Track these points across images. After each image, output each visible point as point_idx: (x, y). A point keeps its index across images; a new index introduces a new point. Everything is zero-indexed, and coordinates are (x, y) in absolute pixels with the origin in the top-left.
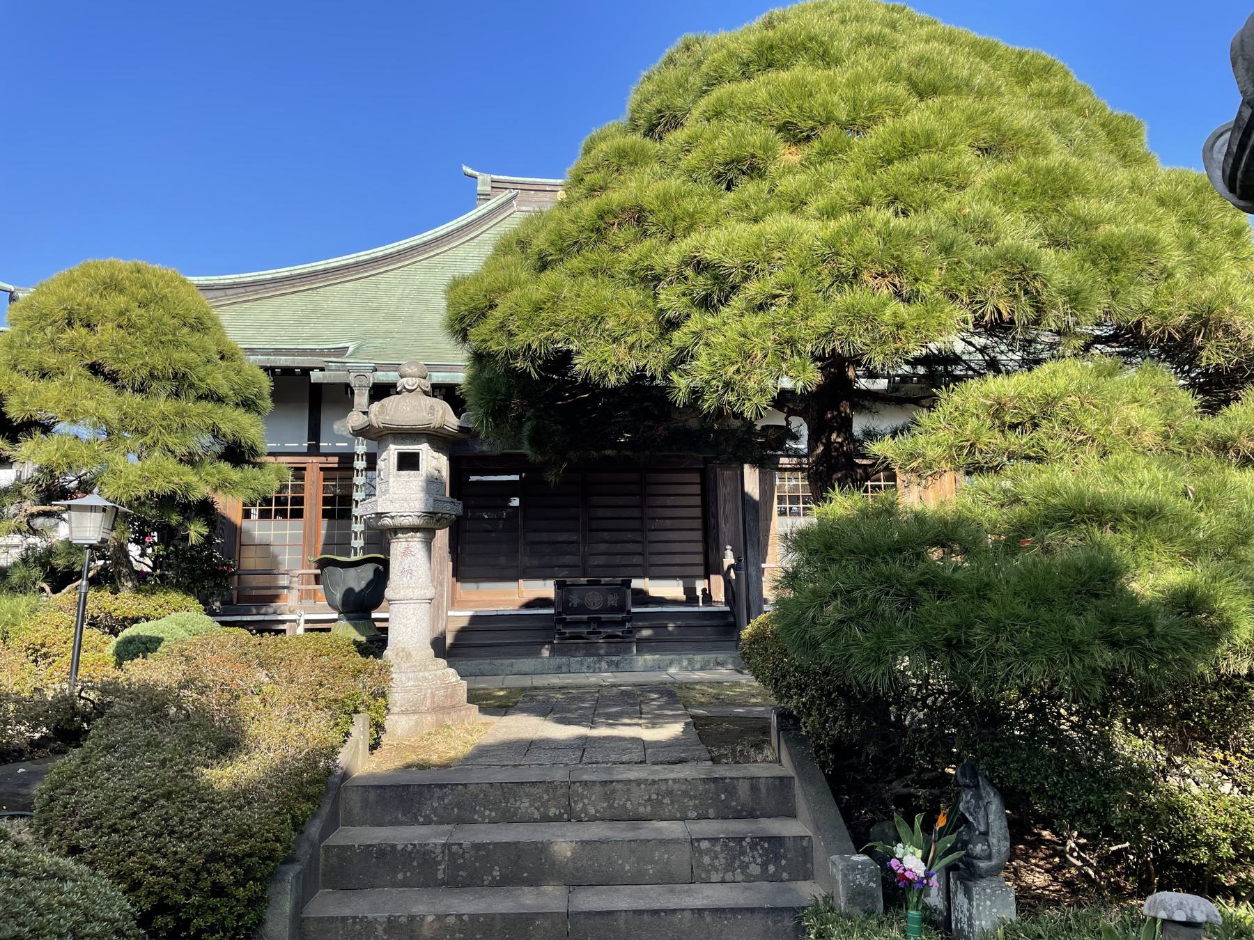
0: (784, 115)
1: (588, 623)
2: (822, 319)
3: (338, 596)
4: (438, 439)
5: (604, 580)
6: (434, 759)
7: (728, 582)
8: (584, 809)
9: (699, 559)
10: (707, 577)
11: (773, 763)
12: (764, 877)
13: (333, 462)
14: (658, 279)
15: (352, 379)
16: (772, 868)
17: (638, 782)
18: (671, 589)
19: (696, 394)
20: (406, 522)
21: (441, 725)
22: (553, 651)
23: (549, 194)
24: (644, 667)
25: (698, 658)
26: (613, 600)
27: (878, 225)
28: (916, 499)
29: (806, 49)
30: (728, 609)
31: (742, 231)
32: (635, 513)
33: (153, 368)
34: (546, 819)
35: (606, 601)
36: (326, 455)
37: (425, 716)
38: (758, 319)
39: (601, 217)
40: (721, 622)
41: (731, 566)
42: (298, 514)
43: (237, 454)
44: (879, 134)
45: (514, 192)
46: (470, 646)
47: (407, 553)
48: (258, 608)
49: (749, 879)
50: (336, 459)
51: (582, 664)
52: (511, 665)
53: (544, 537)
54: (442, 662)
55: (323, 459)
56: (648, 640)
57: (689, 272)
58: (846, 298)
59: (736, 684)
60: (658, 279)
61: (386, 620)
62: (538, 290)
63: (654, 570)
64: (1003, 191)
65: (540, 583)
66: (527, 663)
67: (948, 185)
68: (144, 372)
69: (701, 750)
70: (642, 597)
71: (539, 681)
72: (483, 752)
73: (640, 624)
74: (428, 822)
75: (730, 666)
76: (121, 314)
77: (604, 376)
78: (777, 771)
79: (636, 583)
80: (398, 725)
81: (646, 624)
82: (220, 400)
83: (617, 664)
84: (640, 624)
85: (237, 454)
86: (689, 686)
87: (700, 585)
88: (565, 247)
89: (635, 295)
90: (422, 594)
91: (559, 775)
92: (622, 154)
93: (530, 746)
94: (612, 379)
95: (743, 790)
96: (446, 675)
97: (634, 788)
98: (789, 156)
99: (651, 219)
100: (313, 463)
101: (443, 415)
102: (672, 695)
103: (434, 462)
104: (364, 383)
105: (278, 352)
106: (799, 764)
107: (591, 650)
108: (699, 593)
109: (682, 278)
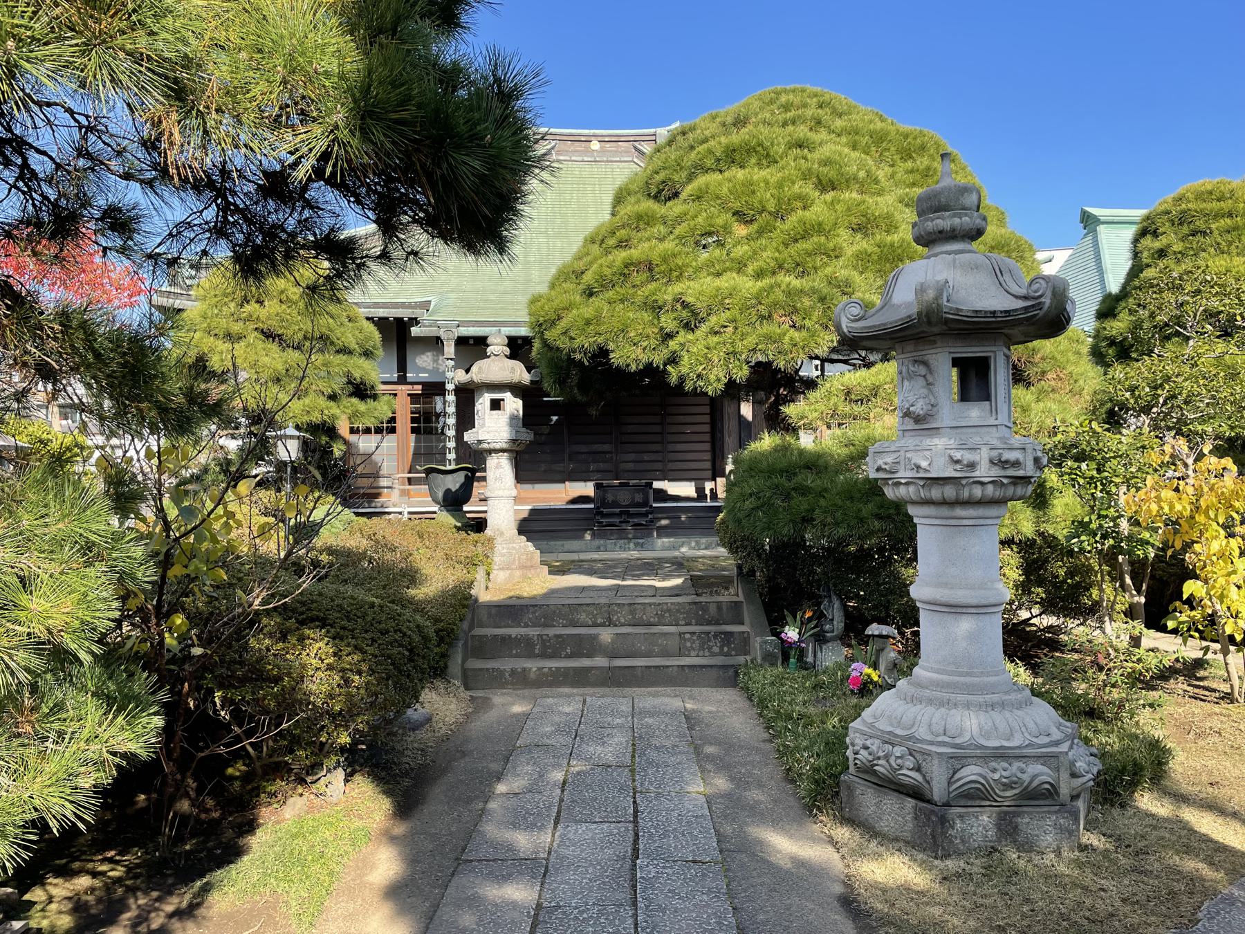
0: (737, 205)
2: (750, 341)
3: (440, 495)
4: (516, 389)
5: (632, 482)
6: (525, 594)
8: (618, 620)
9: (708, 465)
11: (734, 594)
12: (721, 653)
13: (418, 389)
14: (660, 308)
15: (442, 334)
16: (726, 649)
17: (650, 604)
19: (682, 379)
20: (498, 446)
21: (525, 577)
22: (593, 536)
23: (583, 144)
24: (662, 547)
25: (704, 540)
26: (639, 498)
27: (784, 286)
28: (806, 441)
29: (756, 152)
31: (708, 283)
32: (657, 429)
33: (307, 332)
34: (595, 625)
35: (633, 498)
36: (413, 384)
37: (511, 570)
38: (716, 339)
39: (626, 267)
41: (731, 472)
42: (392, 430)
43: (361, 391)
44: (793, 219)
45: (553, 143)
47: (498, 466)
48: (369, 503)
49: (713, 655)
50: (420, 387)
53: (583, 448)
54: (523, 538)
55: (410, 387)
56: (665, 527)
57: (678, 306)
58: (767, 328)
60: (660, 308)
62: (588, 312)
64: (862, 261)
65: (582, 484)
67: (829, 256)
68: (300, 335)
69: (692, 591)
70: (662, 495)
71: (583, 556)
72: (553, 592)
74: (526, 626)
76: (282, 292)
77: (628, 365)
78: (735, 599)
79: (657, 485)
80: (499, 576)
82: (350, 353)
83: (642, 545)
85: (361, 391)
86: (694, 559)
87: (709, 486)
88: (605, 284)
89: (647, 316)
90: (503, 496)
91: (603, 601)
92: (639, 217)
93: (583, 589)
94: (633, 367)
95: (713, 609)
96: (525, 547)
97: (648, 608)
98: (741, 230)
99: (657, 269)
100: (403, 389)
101: (518, 372)
102: (679, 565)
103: (513, 404)
104: (451, 336)
105: (376, 305)
106: (746, 595)
107: (622, 535)
108: (707, 492)
109: (674, 310)
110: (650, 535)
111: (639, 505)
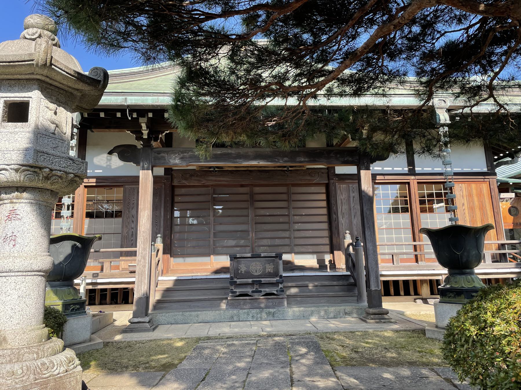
1: (253, 284)
5: (102, 250)
7: (348, 256)
9: (327, 241)
10: (332, 252)
18: (310, 261)
25: (332, 309)
26: (270, 268)
30: (349, 273)
35: (265, 268)
40: (345, 283)
46: (170, 302)
50: (94, 180)
51: (248, 314)
52: (197, 316)
56: (294, 296)
59: (365, 334)
61: (133, 283)
63: (296, 249)
66: (209, 315)
70: (290, 266)
73: (290, 284)
75: (355, 315)
81: (293, 284)
83: (273, 314)
84: (290, 284)
108: (327, 263)
110: (281, 304)
111: (270, 275)
